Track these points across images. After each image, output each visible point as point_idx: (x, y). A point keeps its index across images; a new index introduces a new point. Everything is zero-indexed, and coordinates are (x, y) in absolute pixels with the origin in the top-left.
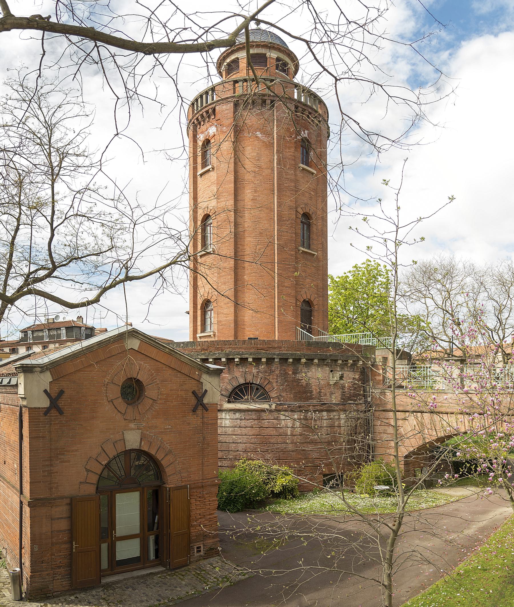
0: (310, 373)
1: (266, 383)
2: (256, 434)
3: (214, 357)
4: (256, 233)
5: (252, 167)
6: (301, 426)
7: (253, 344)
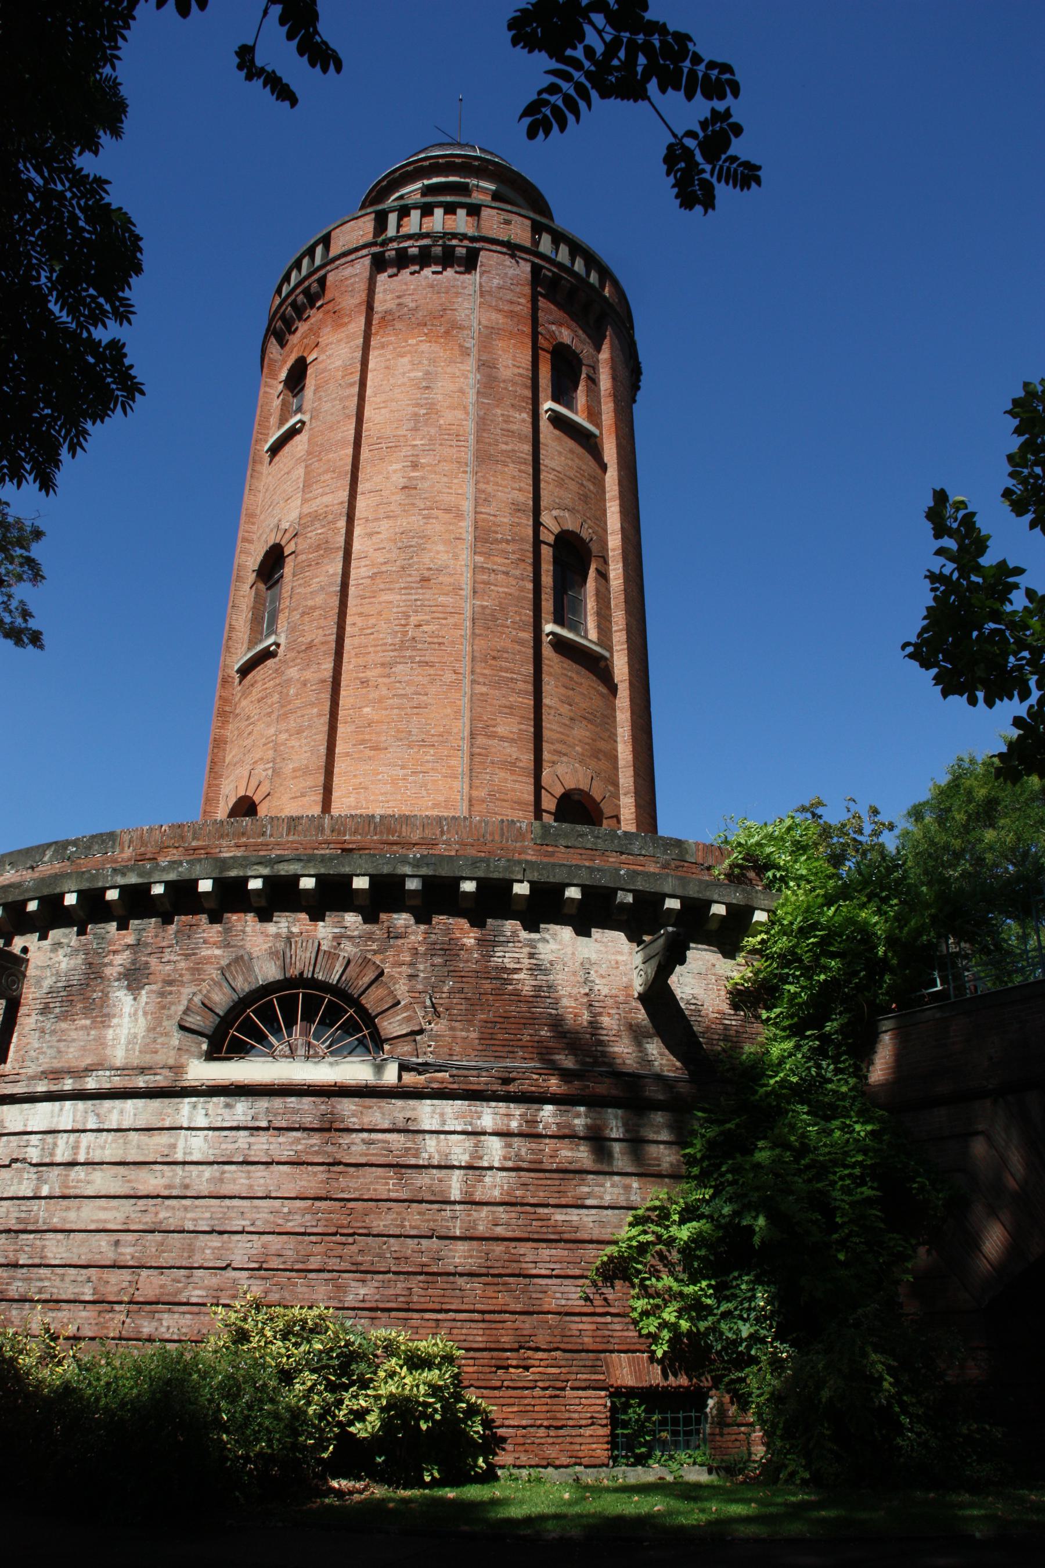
0: (552, 946)
1: (367, 980)
2: (311, 1193)
3: (172, 876)
4: (409, 579)
5: (408, 405)
6: (510, 1164)
7: (327, 831)
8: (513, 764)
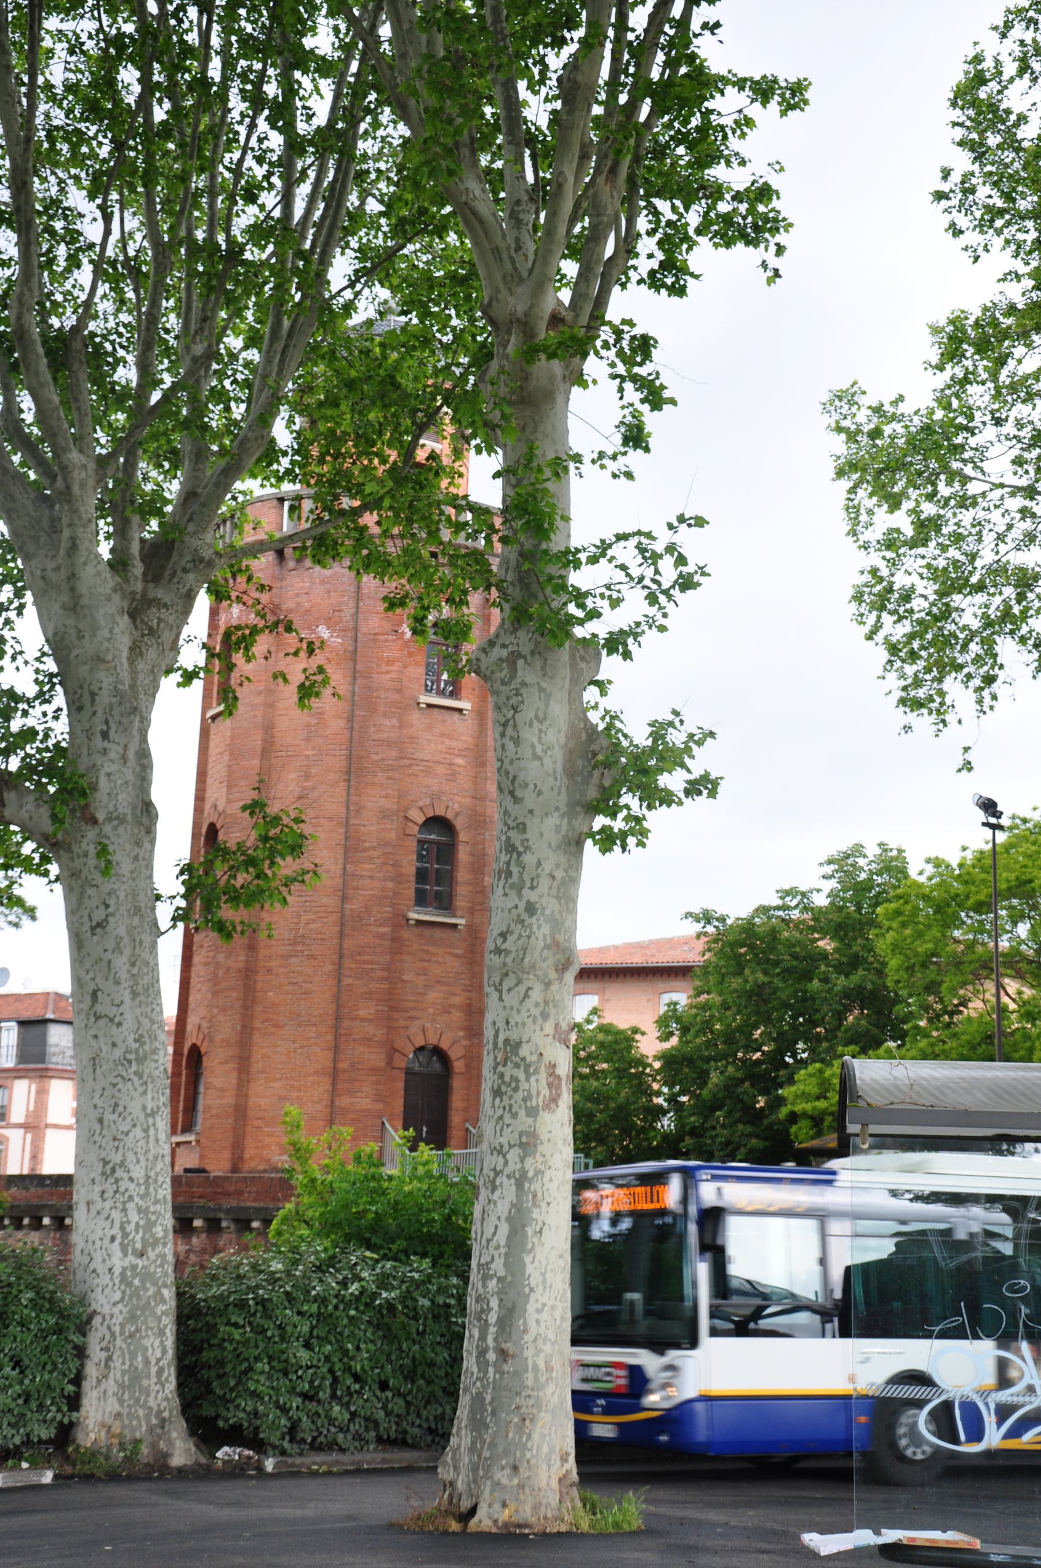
8: (370, 1040)
